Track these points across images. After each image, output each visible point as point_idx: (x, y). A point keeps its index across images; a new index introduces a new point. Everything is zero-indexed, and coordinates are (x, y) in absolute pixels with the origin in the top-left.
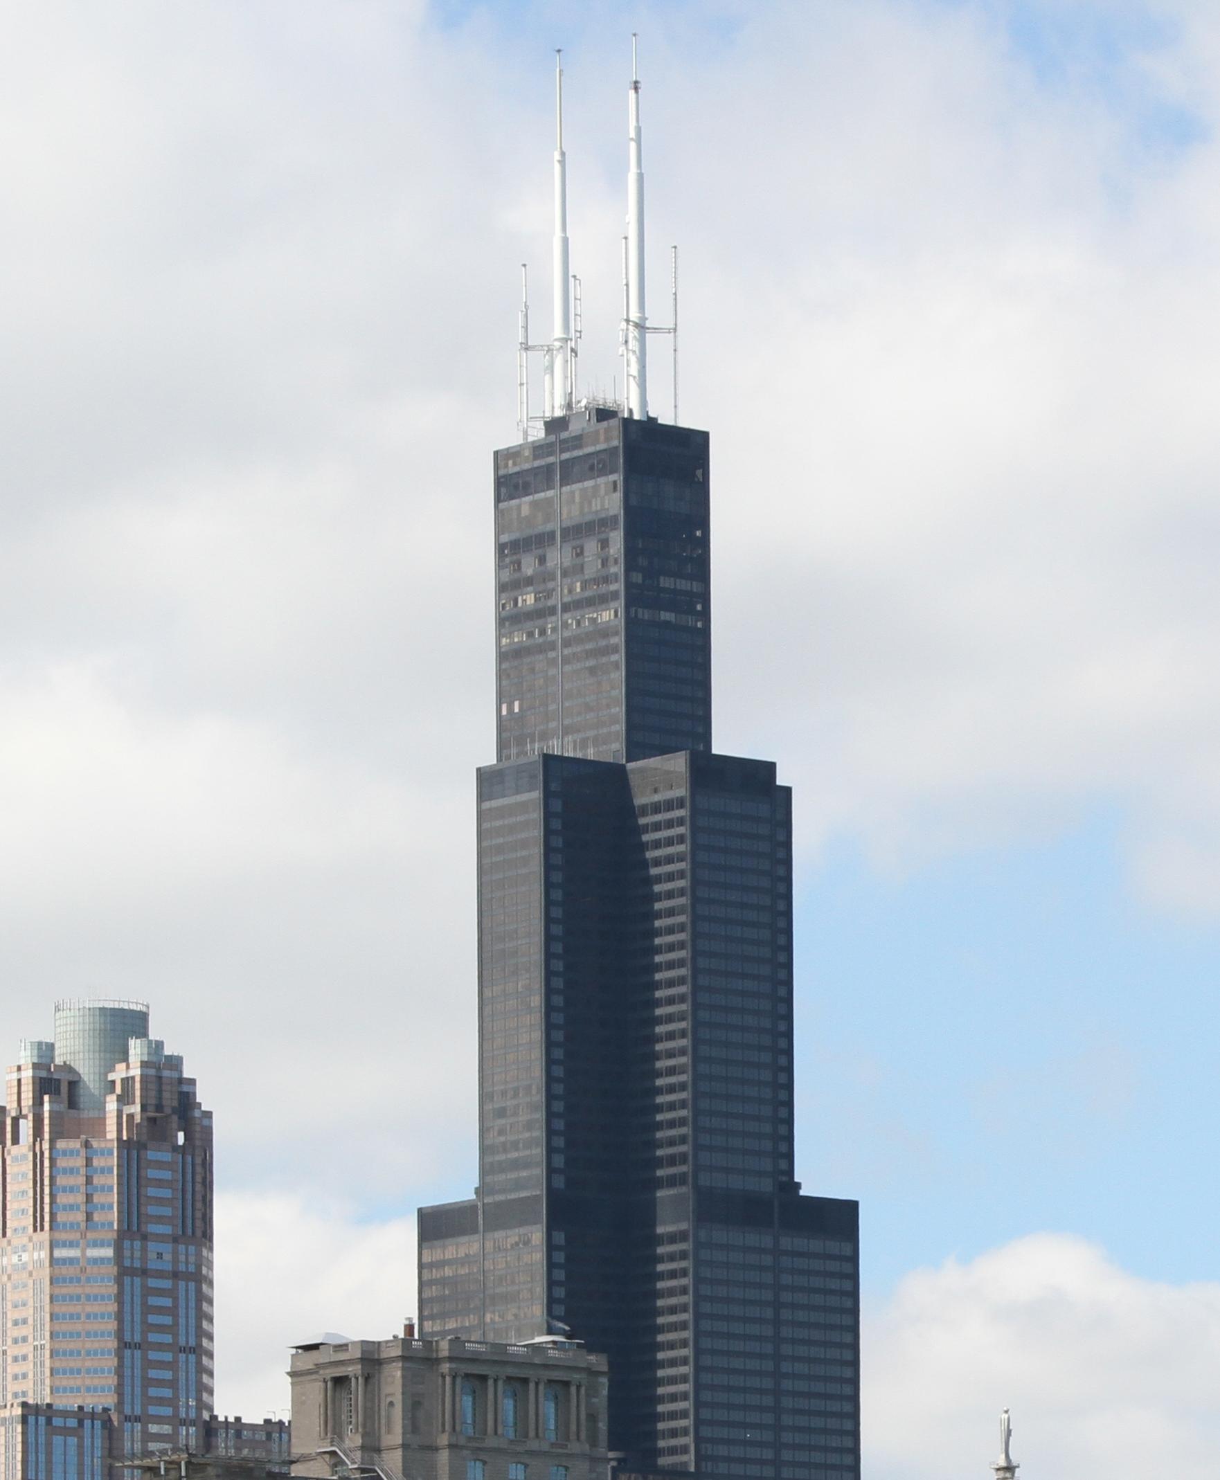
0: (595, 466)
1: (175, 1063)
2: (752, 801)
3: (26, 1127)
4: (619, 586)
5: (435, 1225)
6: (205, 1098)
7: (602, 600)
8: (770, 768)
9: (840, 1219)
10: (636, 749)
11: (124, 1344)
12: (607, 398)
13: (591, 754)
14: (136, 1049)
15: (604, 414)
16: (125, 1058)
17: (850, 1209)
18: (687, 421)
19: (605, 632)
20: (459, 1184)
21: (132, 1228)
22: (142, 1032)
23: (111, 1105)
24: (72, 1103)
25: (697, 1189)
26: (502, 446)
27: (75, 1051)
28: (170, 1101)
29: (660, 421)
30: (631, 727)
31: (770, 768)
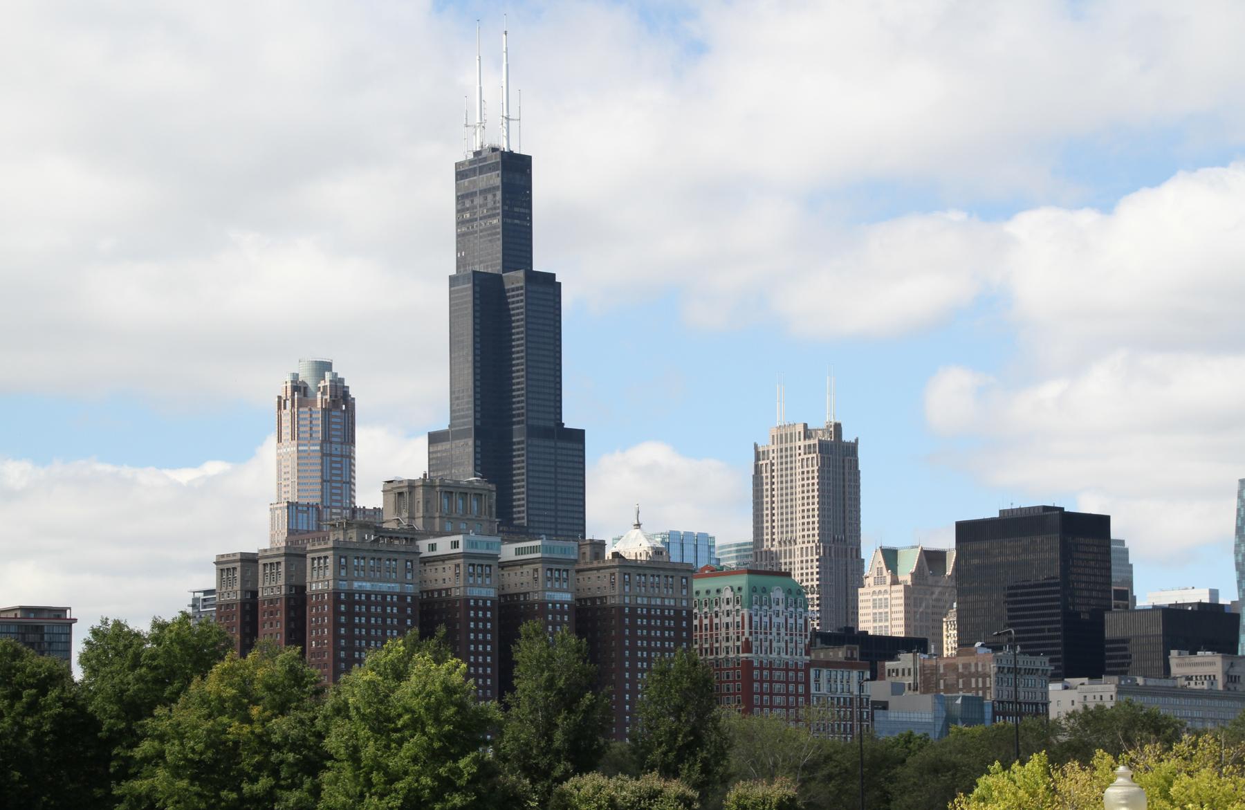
0: (491, 168)
1: (342, 380)
2: (547, 287)
3: (289, 403)
5: (434, 438)
6: (352, 393)
7: (494, 216)
8: (554, 275)
10: (506, 268)
11: (323, 481)
12: (496, 144)
13: (490, 271)
14: (328, 375)
15: (494, 150)
19: (495, 227)
20: (443, 424)
21: (326, 439)
22: (330, 370)
24: (305, 395)
28: (340, 394)
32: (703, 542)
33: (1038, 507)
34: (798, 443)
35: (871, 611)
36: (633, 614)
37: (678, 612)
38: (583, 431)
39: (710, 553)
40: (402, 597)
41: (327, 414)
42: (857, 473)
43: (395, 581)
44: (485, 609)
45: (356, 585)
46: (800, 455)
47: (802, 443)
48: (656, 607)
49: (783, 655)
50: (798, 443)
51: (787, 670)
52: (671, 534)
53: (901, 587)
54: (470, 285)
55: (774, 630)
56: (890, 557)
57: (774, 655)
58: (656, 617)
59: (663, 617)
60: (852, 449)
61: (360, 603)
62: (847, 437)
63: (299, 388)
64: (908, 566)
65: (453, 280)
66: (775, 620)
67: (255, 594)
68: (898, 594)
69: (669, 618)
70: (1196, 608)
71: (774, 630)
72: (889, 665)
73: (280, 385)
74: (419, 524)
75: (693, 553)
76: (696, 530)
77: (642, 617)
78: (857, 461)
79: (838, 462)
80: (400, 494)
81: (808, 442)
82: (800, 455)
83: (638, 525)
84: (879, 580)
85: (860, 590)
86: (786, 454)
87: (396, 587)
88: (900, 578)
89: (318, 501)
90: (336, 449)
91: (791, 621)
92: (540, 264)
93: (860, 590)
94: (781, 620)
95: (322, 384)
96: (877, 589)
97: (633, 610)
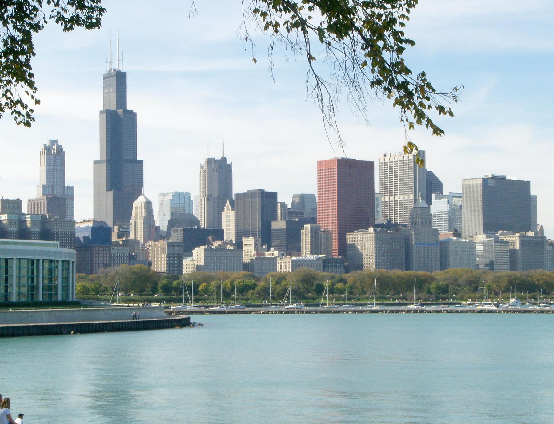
0: (113, 76)
2: (132, 115)
5: (95, 163)
9: (141, 162)
10: (117, 108)
12: (115, 68)
15: (115, 70)
17: (143, 161)
18: (124, 71)
20: (98, 159)
26: (426, 153)
30: (117, 106)
36: (58, 234)
37: (71, 233)
38: (276, 193)
41: (54, 157)
44: (36, 234)
59: (67, 234)
70: (109, 165)
73: (42, 148)
76: (185, 191)
92: (129, 108)
97: (57, 233)
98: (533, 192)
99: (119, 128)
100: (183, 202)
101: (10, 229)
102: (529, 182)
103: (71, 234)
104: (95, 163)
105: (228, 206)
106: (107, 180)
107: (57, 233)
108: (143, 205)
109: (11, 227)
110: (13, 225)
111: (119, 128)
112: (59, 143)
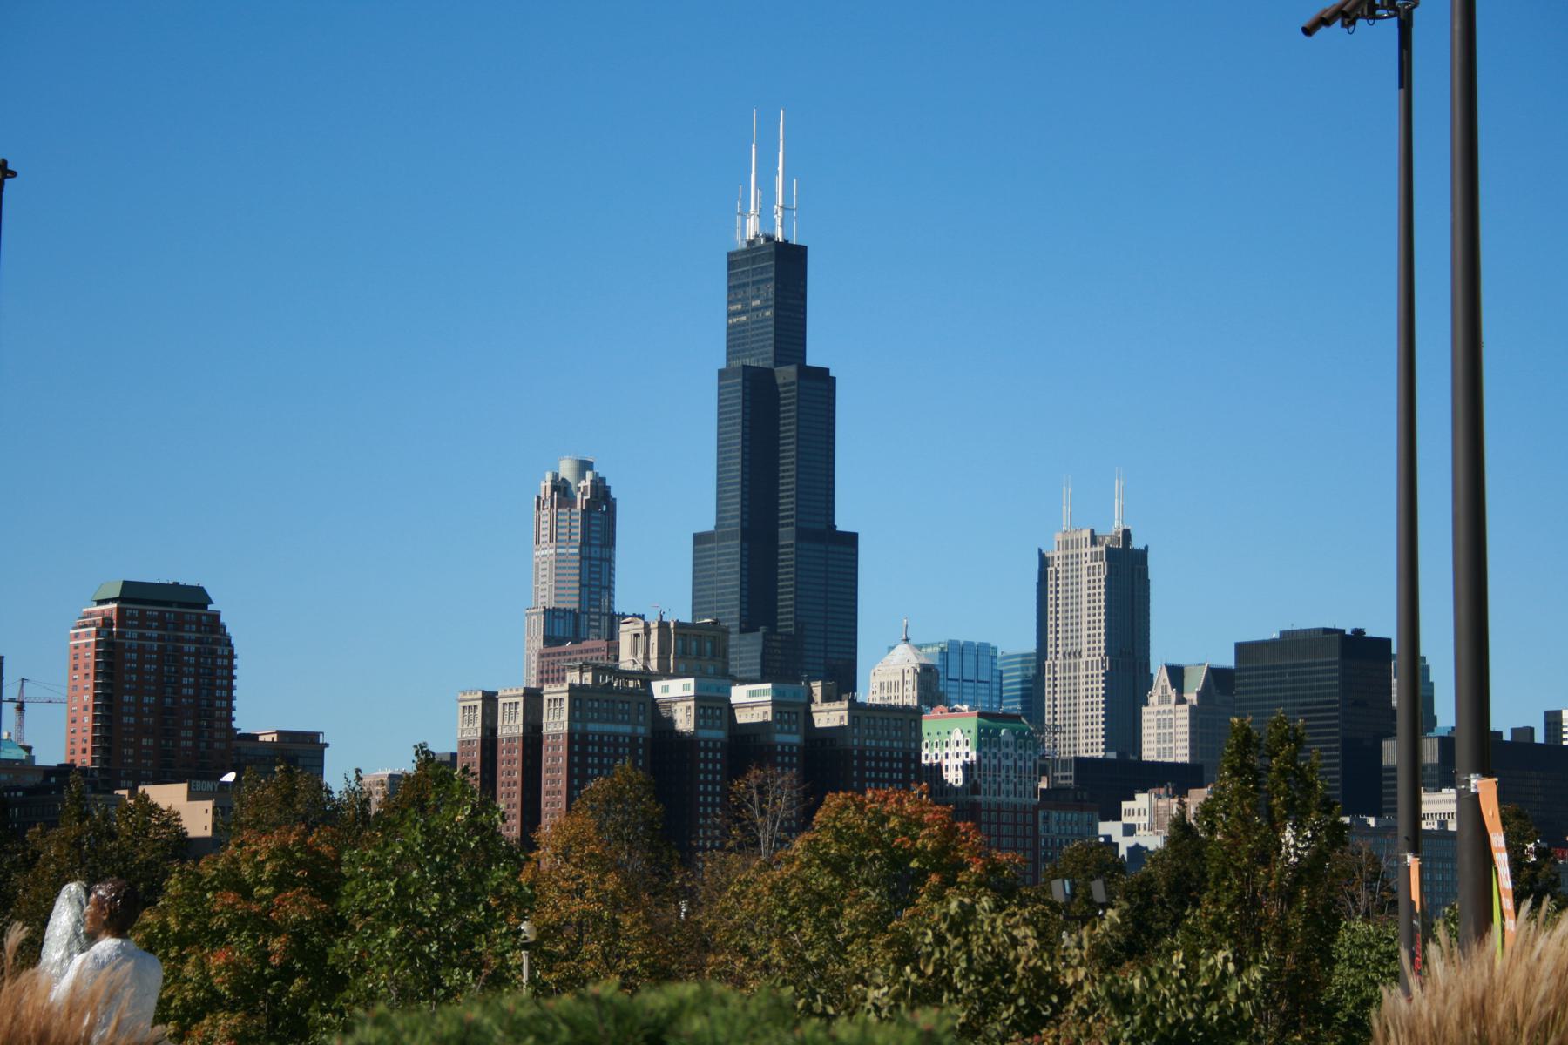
1: (603, 480)
2: (822, 382)
3: (548, 504)
4: (771, 303)
5: (699, 539)
6: (614, 493)
7: (767, 308)
8: (827, 371)
9: (851, 539)
10: (778, 363)
11: (581, 586)
13: (761, 364)
14: (589, 475)
16: (584, 478)
19: (767, 319)
20: (709, 524)
21: (586, 542)
22: (591, 469)
23: (579, 496)
24: (565, 495)
25: (797, 528)
27: (566, 470)
28: (601, 494)
29: (1368, 634)
31: (827, 371)
32: (984, 652)
33: (1314, 630)
34: (1084, 550)
35: (1155, 731)
36: (862, 757)
39: (993, 664)
40: (634, 738)
42: (1147, 582)
43: (627, 723)
44: (715, 750)
45: (591, 727)
46: (1086, 563)
47: (1088, 550)
48: (884, 749)
49: (1011, 797)
50: (1084, 550)
51: (1016, 812)
52: (951, 643)
53: (1186, 707)
54: (740, 380)
55: (1003, 773)
56: (1177, 675)
57: (1003, 797)
58: (884, 760)
59: (891, 760)
60: (1142, 555)
61: (593, 743)
62: (1136, 544)
63: (561, 489)
64: (1194, 685)
65: (722, 374)
66: (1004, 762)
67: (495, 730)
68: (1183, 712)
69: (898, 760)
71: (1003, 773)
72: (1125, 805)
74: (653, 665)
75: (973, 665)
76: (977, 638)
77: (870, 759)
78: (1146, 570)
79: (1127, 573)
80: (637, 635)
81: (1094, 549)
82: (1086, 563)
83: (907, 640)
84: (1164, 700)
85: (1144, 709)
86: (1073, 560)
87: (627, 729)
88: (1187, 696)
89: (576, 606)
90: (595, 552)
91: (1020, 763)
93: (1144, 709)
94: (1010, 762)
95: (582, 484)
96: (1162, 708)
97: (862, 752)
98: (1269, 632)
99: (780, 423)
100: (957, 676)
101: (779, 738)
102: (805, 248)
103: (907, 756)
104: (699, 539)
105: (1164, 689)
106: (1305, 631)
107: (862, 752)
108: (909, 677)
109: (782, 731)
110: (789, 722)
111: (780, 423)
112: (601, 469)
